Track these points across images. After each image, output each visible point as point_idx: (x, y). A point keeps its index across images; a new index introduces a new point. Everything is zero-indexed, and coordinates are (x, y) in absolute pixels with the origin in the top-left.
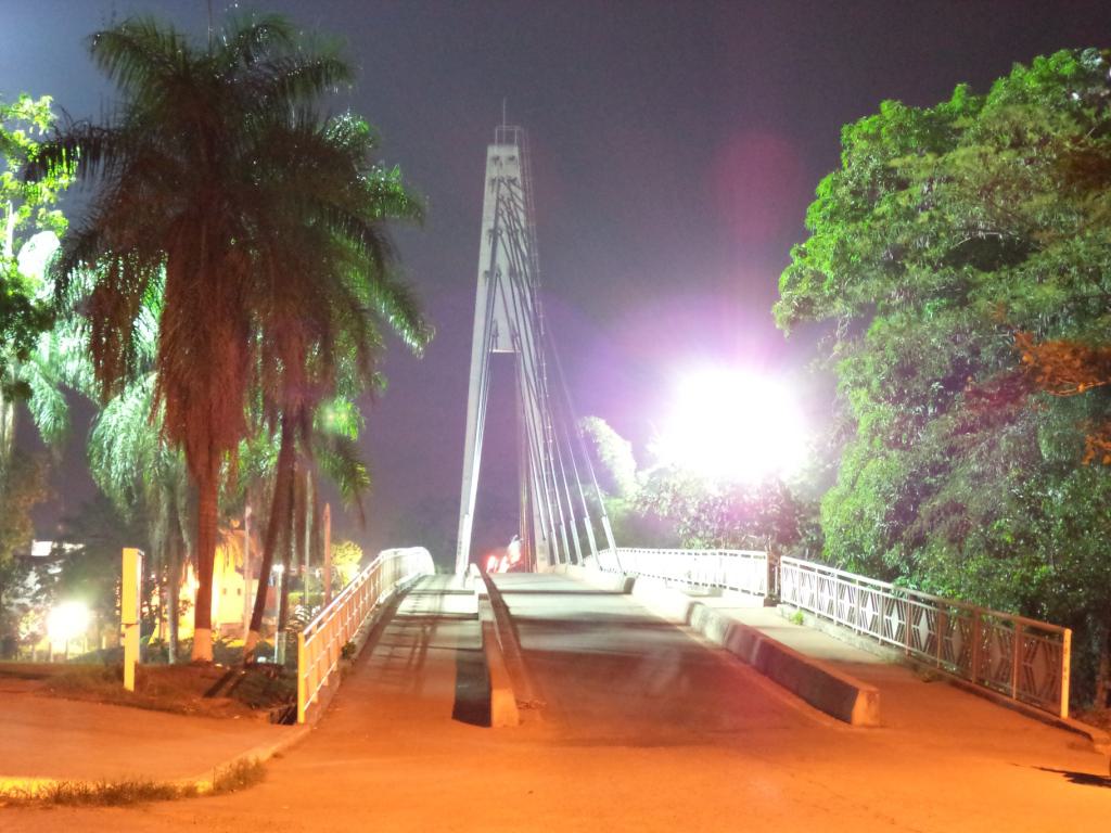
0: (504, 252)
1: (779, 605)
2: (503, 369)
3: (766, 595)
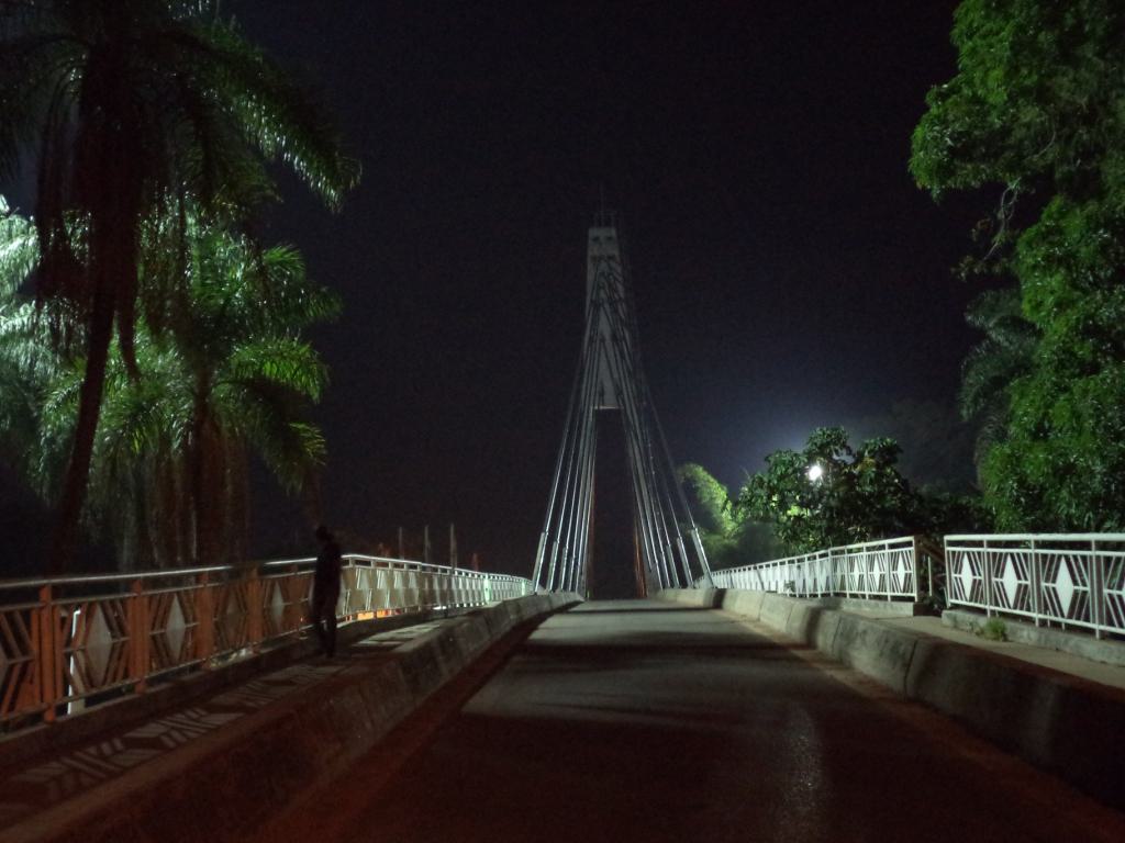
2: (611, 428)
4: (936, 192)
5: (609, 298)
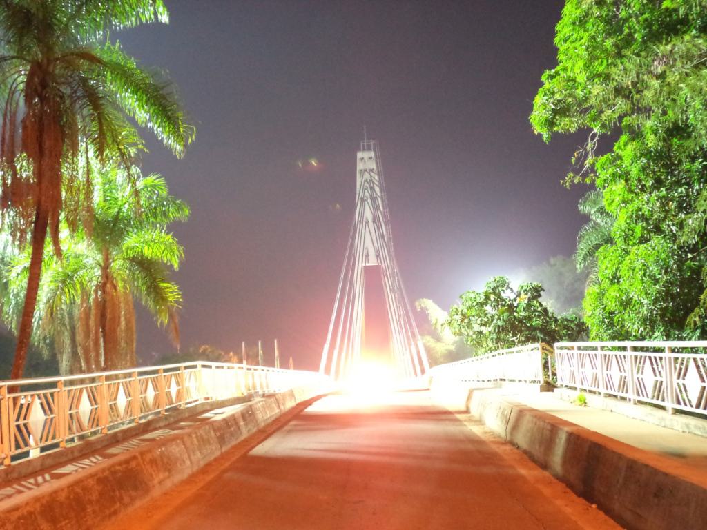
0: (369, 209)
1: (555, 389)
3: (542, 382)
4: (545, 137)
5: (371, 195)
